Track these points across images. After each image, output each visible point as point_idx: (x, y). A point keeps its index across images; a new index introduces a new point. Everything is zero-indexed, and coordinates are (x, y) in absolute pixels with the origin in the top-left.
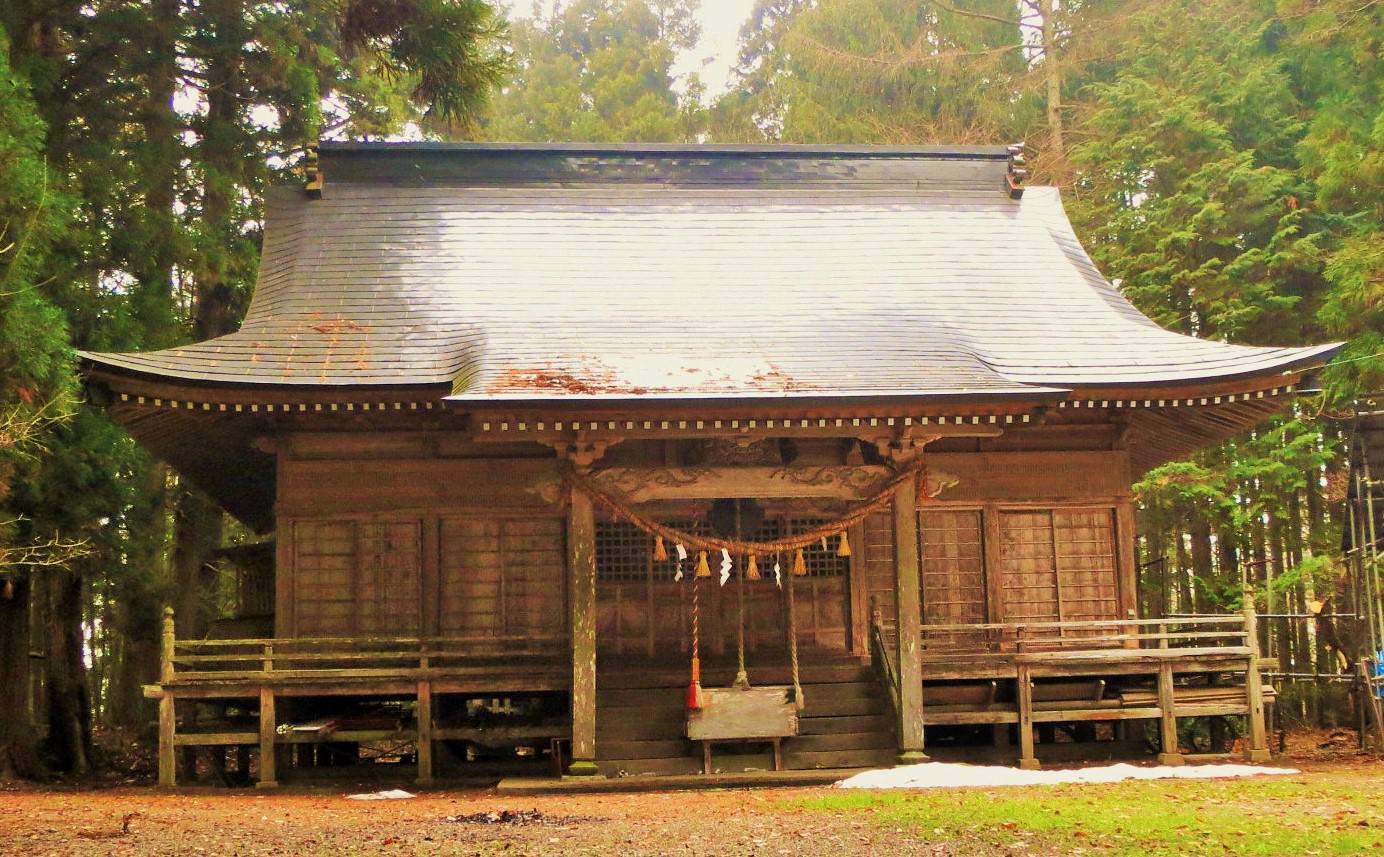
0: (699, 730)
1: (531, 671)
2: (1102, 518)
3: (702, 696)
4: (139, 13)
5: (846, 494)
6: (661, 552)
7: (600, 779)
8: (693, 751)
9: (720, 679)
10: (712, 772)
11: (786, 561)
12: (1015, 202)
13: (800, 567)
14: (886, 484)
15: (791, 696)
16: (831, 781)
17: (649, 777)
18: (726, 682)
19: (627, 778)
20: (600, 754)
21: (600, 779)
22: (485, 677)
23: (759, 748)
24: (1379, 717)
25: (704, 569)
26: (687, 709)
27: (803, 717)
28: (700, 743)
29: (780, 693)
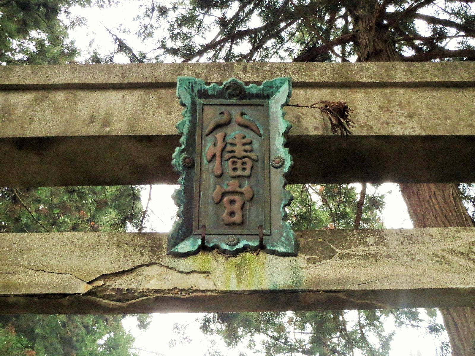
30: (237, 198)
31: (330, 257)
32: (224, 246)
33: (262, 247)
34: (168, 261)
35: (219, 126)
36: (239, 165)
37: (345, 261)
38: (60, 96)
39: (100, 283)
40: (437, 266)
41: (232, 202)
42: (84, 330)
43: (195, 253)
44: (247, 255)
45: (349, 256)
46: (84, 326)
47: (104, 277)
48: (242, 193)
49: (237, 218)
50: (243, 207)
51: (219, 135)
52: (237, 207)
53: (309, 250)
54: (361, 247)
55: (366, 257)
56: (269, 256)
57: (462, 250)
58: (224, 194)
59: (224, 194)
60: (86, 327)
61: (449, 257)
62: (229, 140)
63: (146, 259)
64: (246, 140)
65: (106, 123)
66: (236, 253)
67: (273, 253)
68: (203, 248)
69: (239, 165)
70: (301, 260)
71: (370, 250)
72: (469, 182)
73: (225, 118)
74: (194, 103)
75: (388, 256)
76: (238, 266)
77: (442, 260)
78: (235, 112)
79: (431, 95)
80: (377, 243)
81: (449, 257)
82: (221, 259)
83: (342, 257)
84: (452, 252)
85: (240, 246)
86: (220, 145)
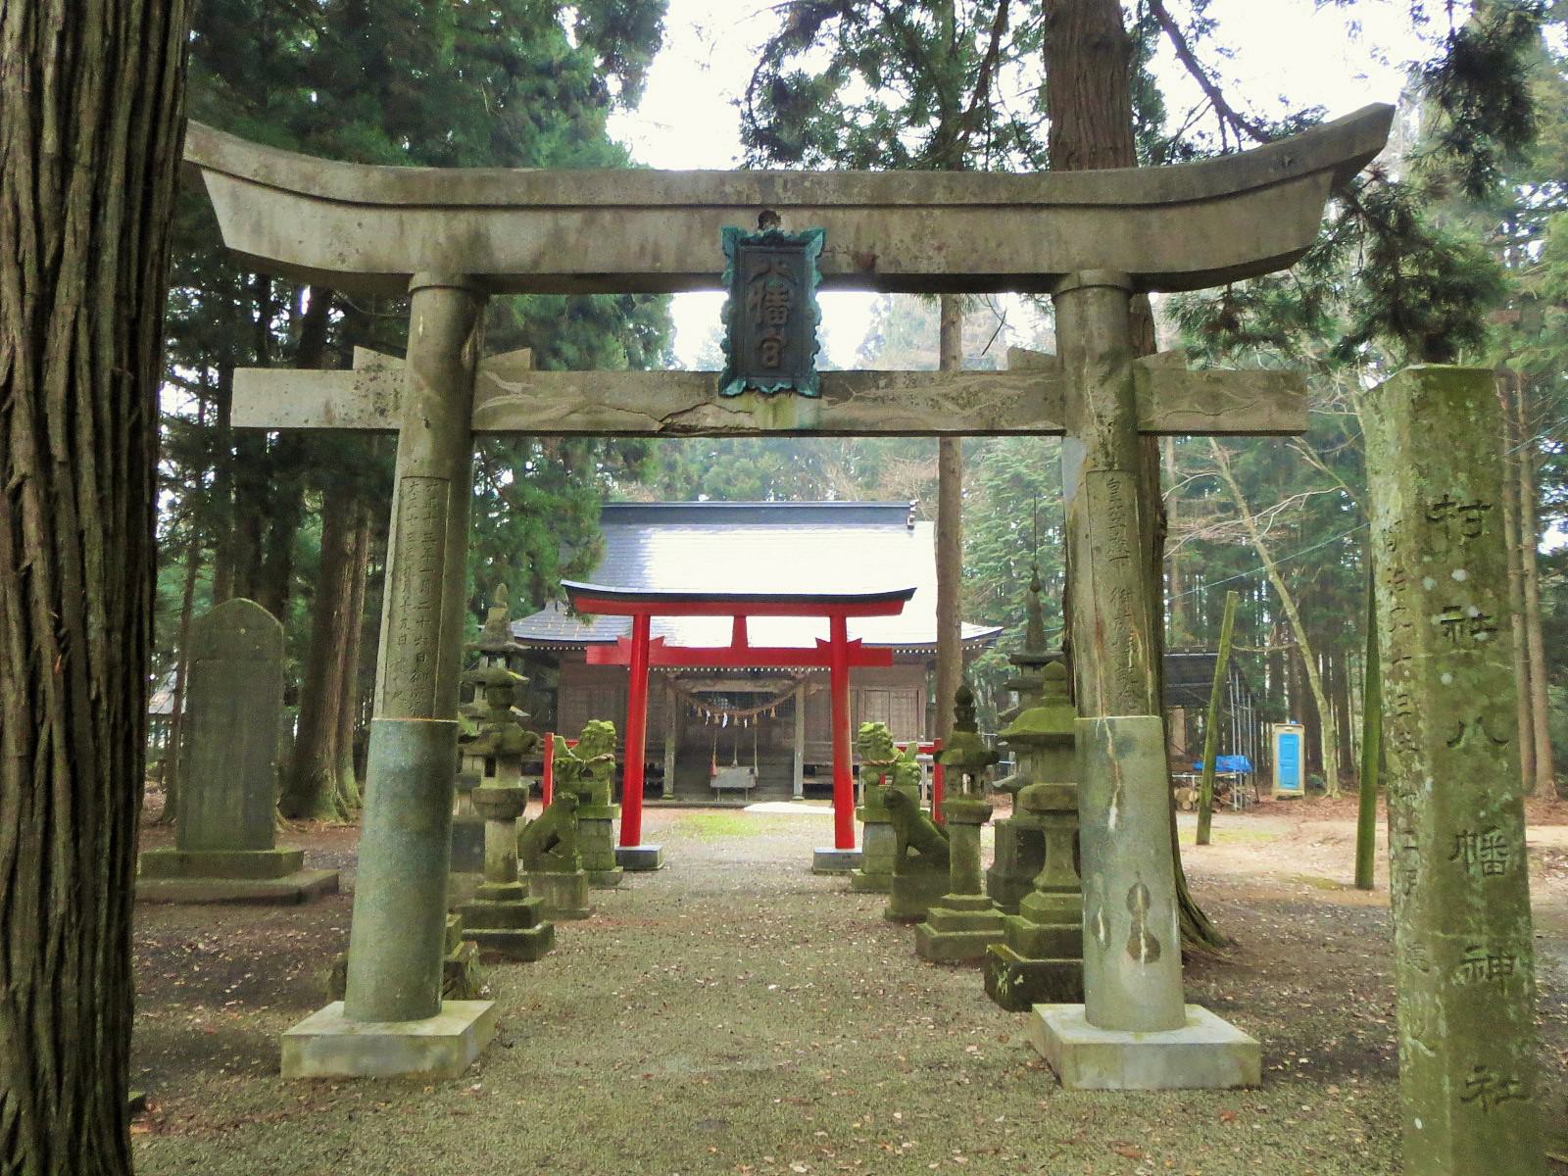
0: (714, 784)
1: (1385, 826)
2: (913, 695)
3: (716, 770)
4: (173, 457)
5: (776, 691)
6: (700, 714)
7: (674, 802)
8: (713, 792)
9: (725, 762)
10: (718, 801)
11: (749, 719)
12: (1078, 741)
13: (755, 720)
14: (792, 688)
15: (752, 771)
16: (742, 807)
17: (694, 802)
18: (728, 764)
19: (687, 801)
20: (675, 791)
21: (674, 802)
22: (340, 735)
23: (739, 792)
24: (4, 237)
25: (717, 721)
26: (710, 776)
27: (757, 780)
28: (812, 792)
29: (747, 770)
30: (775, 345)
31: (847, 399)
32: (764, 389)
33: (793, 390)
34: (719, 401)
35: (760, 275)
36: (776, 314)
37: (858, 404)
38: (607, 217)
39: (669, 420)
40: (929, 410)
41: (770, 348)
42: (532, 125)
43: (740, 394)
44: (782, 396)
45: (862, 399)
46: (532, 118)
47: (671, 415)
48: (778, 341)
49: (773, 363)
50: (779, 353)
51: (760, 284)
52: (774, 352)
53: (831, 393)
54: (873, 390)
55: (876, 399)
56: (800, 398)
57: (954, 394)
58: (764, 342)
59: (764, 342)
60: (537, 120)
61: (942, 401)
62: (769, 289)
63: (702, 399)
64: (784, 289)
65: (656, 258)
66: (773, 395)
67: (803, 395)
68: (747, 389)
69: (776, 314)
70: (824, 402)
71: (880, 393)
72: (1119, 13)
73: (765, 266)
74: (737, 250)
75: (893, 399)
76: (775, 407)
77: (935, 404)
78: (775, 259)
79: (966, 217)
80: (887, 386)
81: (942, 401)
82: (761, 400)
83: (857, 399)
84: (946, 396)
85: (776, 389)
86: (760, 296)
